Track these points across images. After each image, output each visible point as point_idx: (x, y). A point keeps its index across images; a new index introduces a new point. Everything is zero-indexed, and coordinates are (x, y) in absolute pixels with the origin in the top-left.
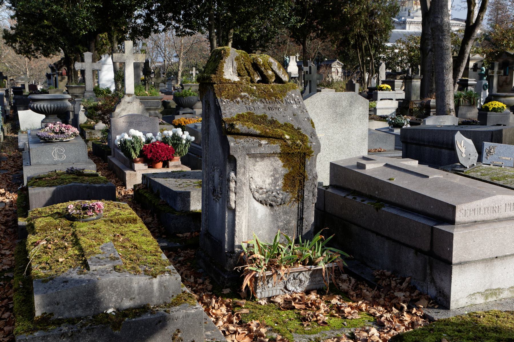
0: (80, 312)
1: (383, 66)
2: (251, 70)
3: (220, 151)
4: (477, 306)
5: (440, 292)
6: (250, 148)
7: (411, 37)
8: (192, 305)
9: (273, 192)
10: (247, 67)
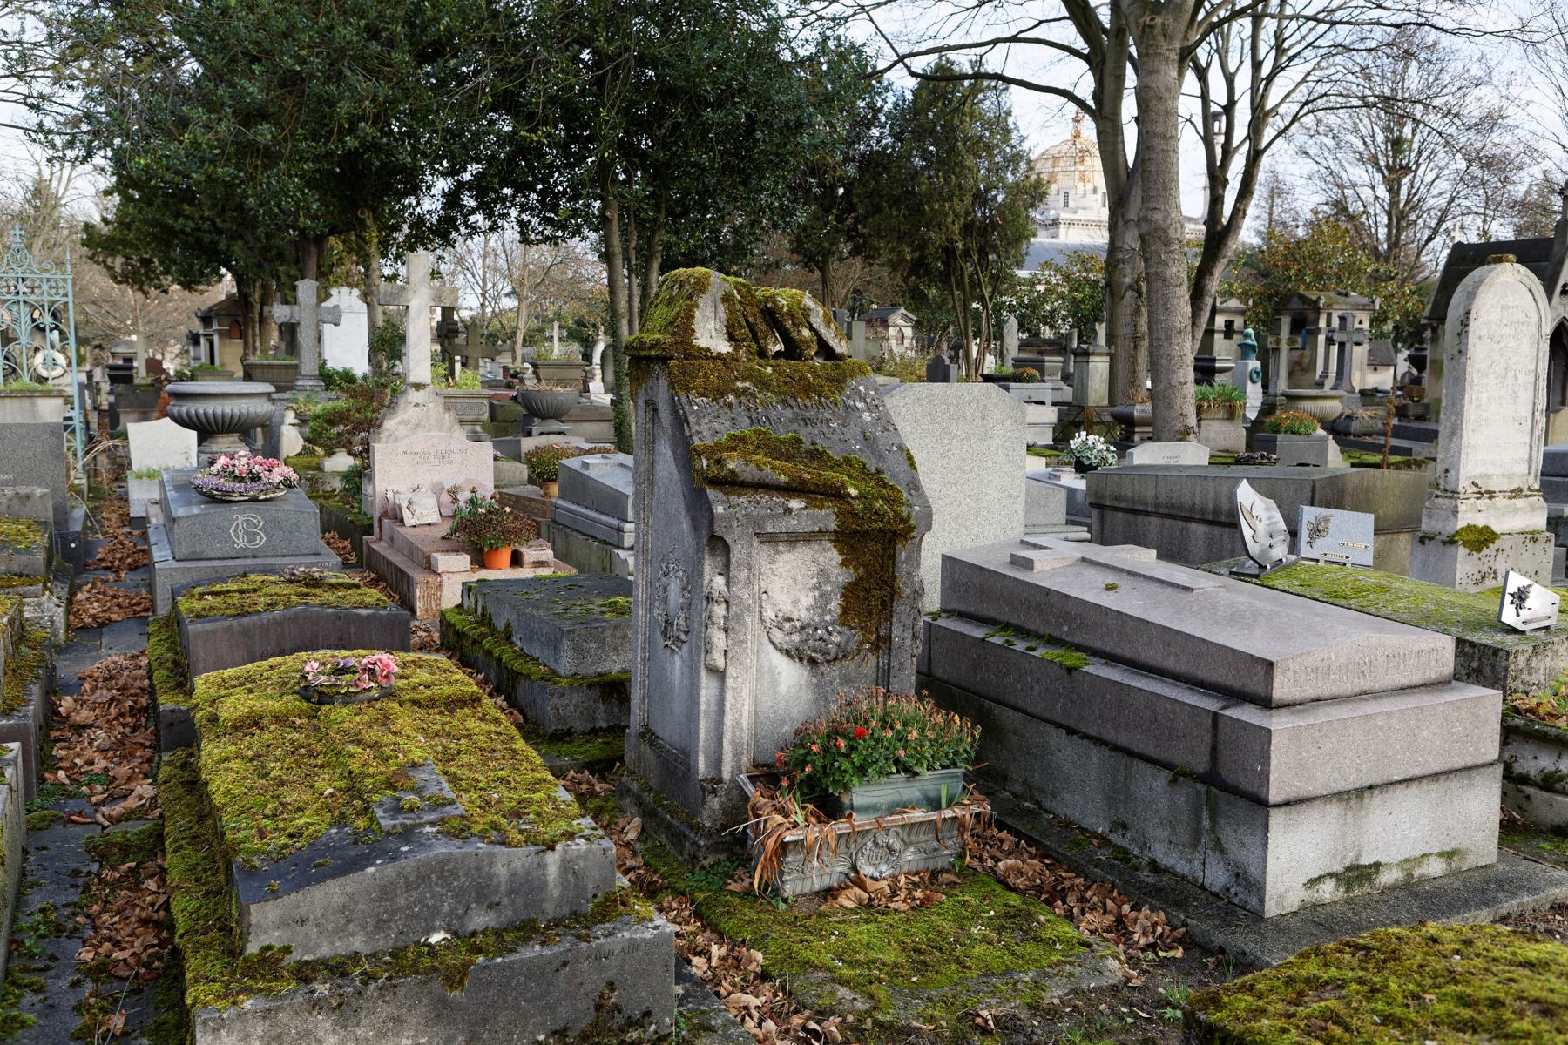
0: (358, 944)
1: (1013, 323)
2: (762, 327)
3: (686, 526)
4: (1328, 909)
5: (1237, 875)
6: (763, 518)
7: (1079, 256)
8: (644, 919)
9: (816, 629)
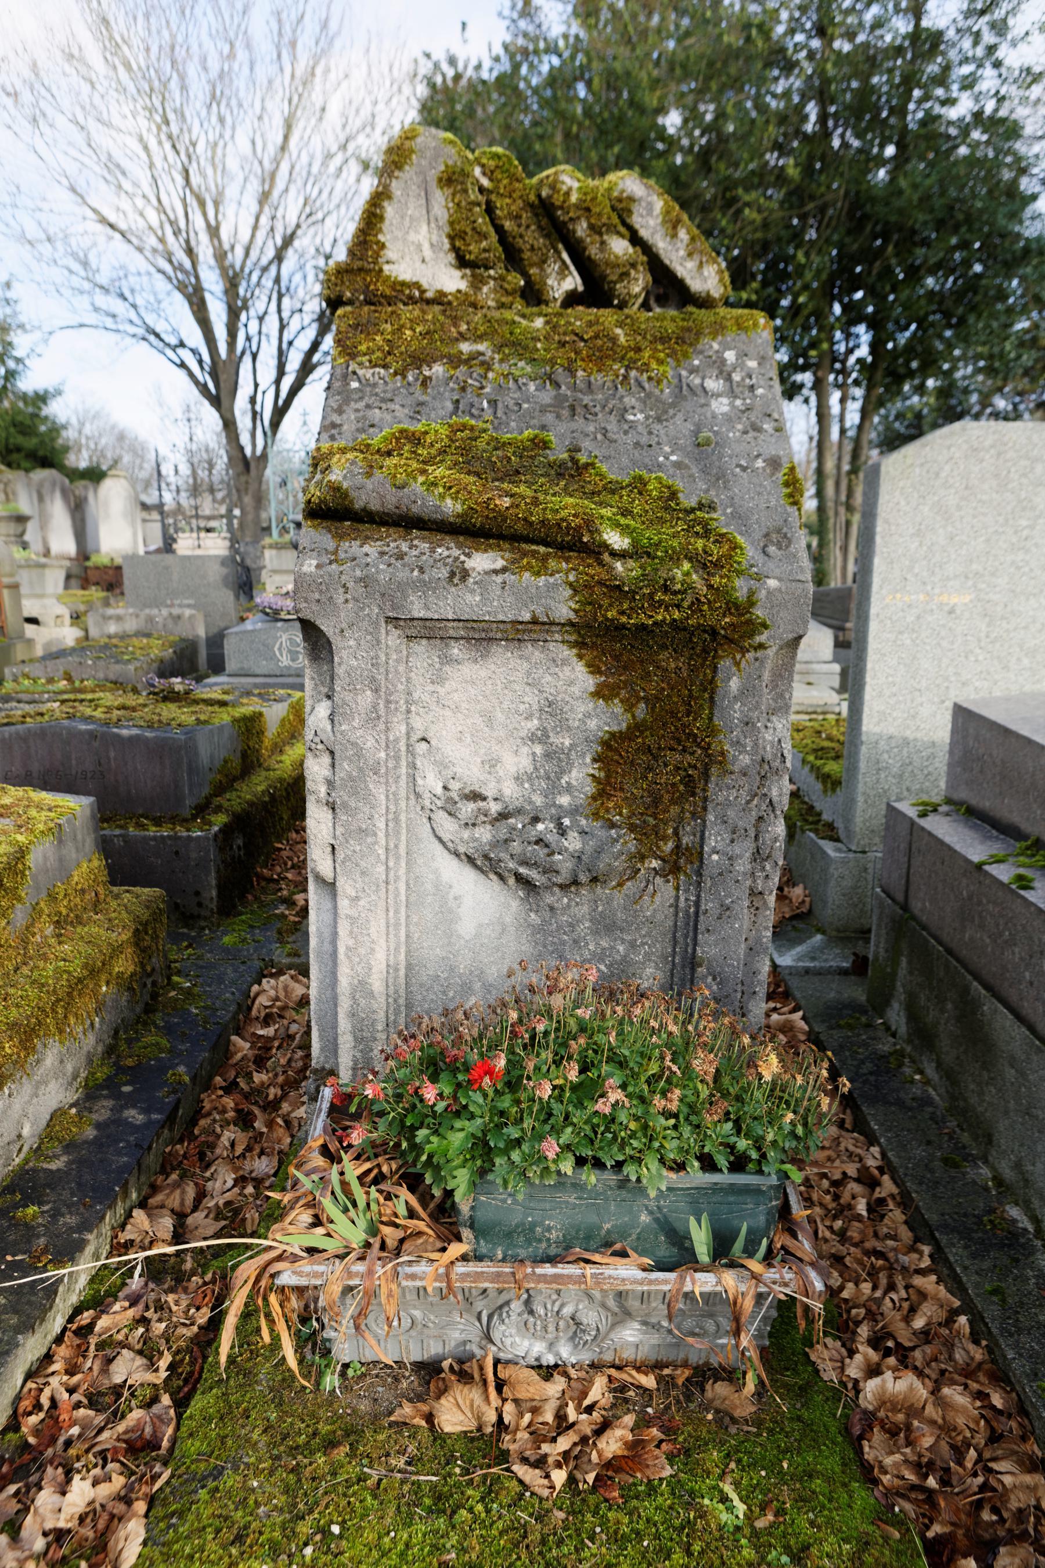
2: (531, 238)
6: (402, 587)
9: (536, 820)
10: (508, 225)
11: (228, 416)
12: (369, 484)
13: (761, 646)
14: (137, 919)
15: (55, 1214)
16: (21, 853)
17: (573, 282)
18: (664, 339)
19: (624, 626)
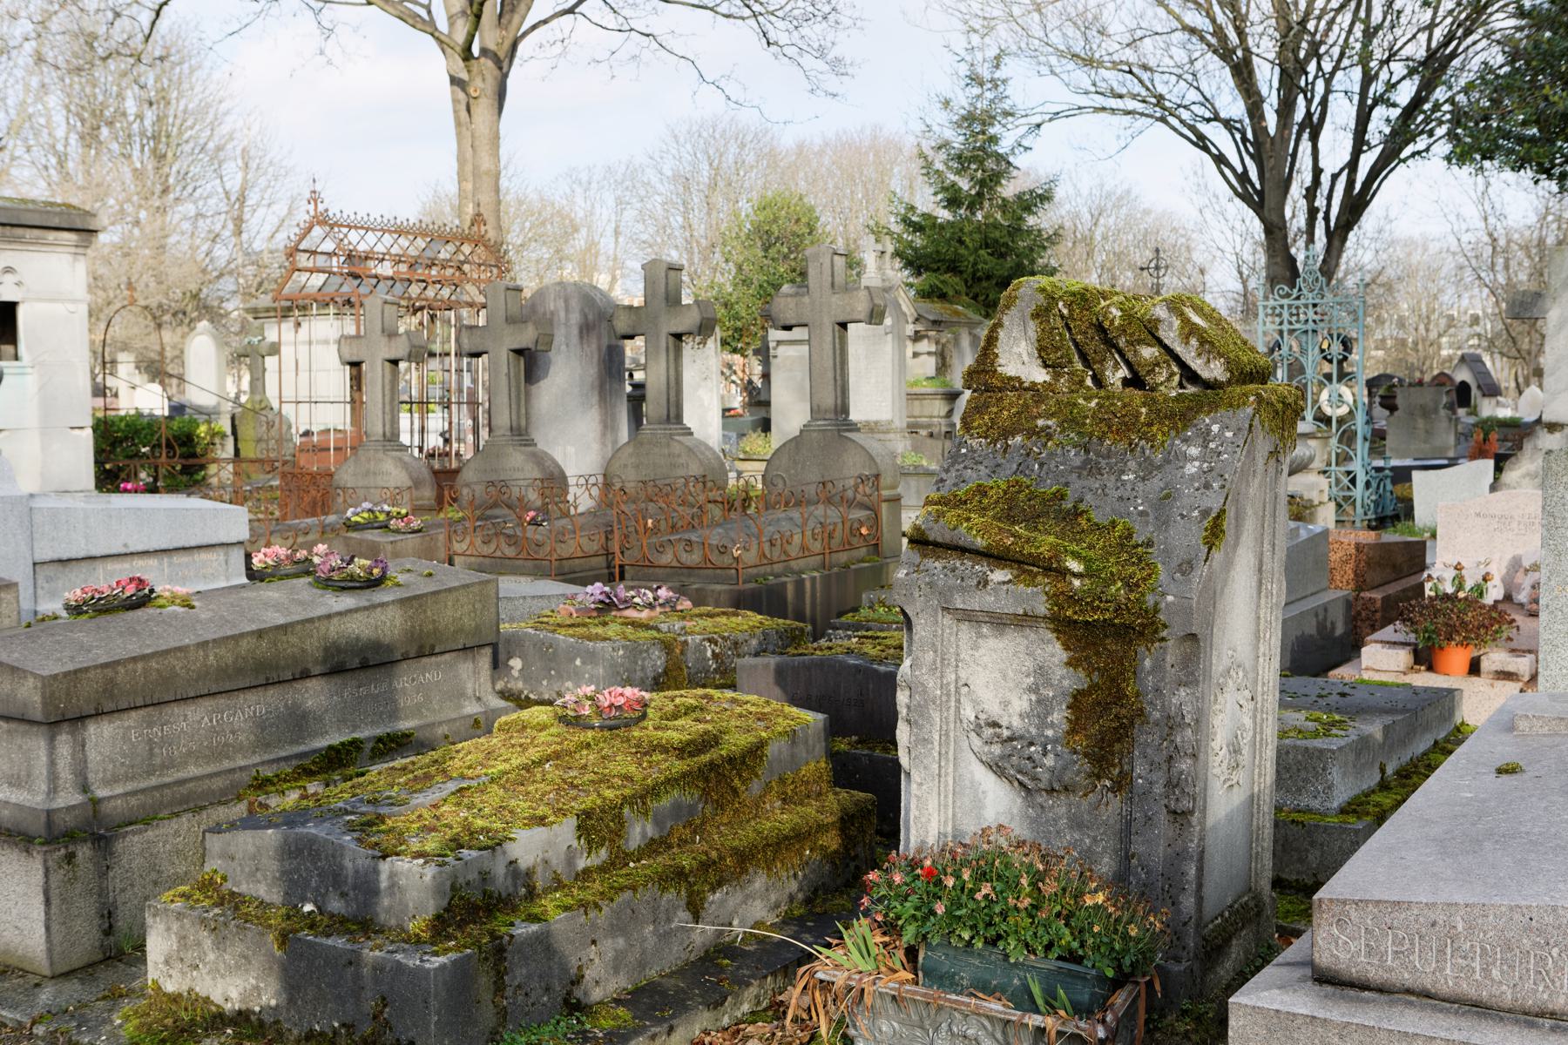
2: (1094, 345)
6: (951, 589)
9: (1031, 744)
11: (1274, 218)
12: (936, 527)
13: (1163, 639)
14: (843, 810)
15: (738, 968)
16: (762, 744)
17: (1123, 372)
18: (1171, 416)
19: (1075, 622)
